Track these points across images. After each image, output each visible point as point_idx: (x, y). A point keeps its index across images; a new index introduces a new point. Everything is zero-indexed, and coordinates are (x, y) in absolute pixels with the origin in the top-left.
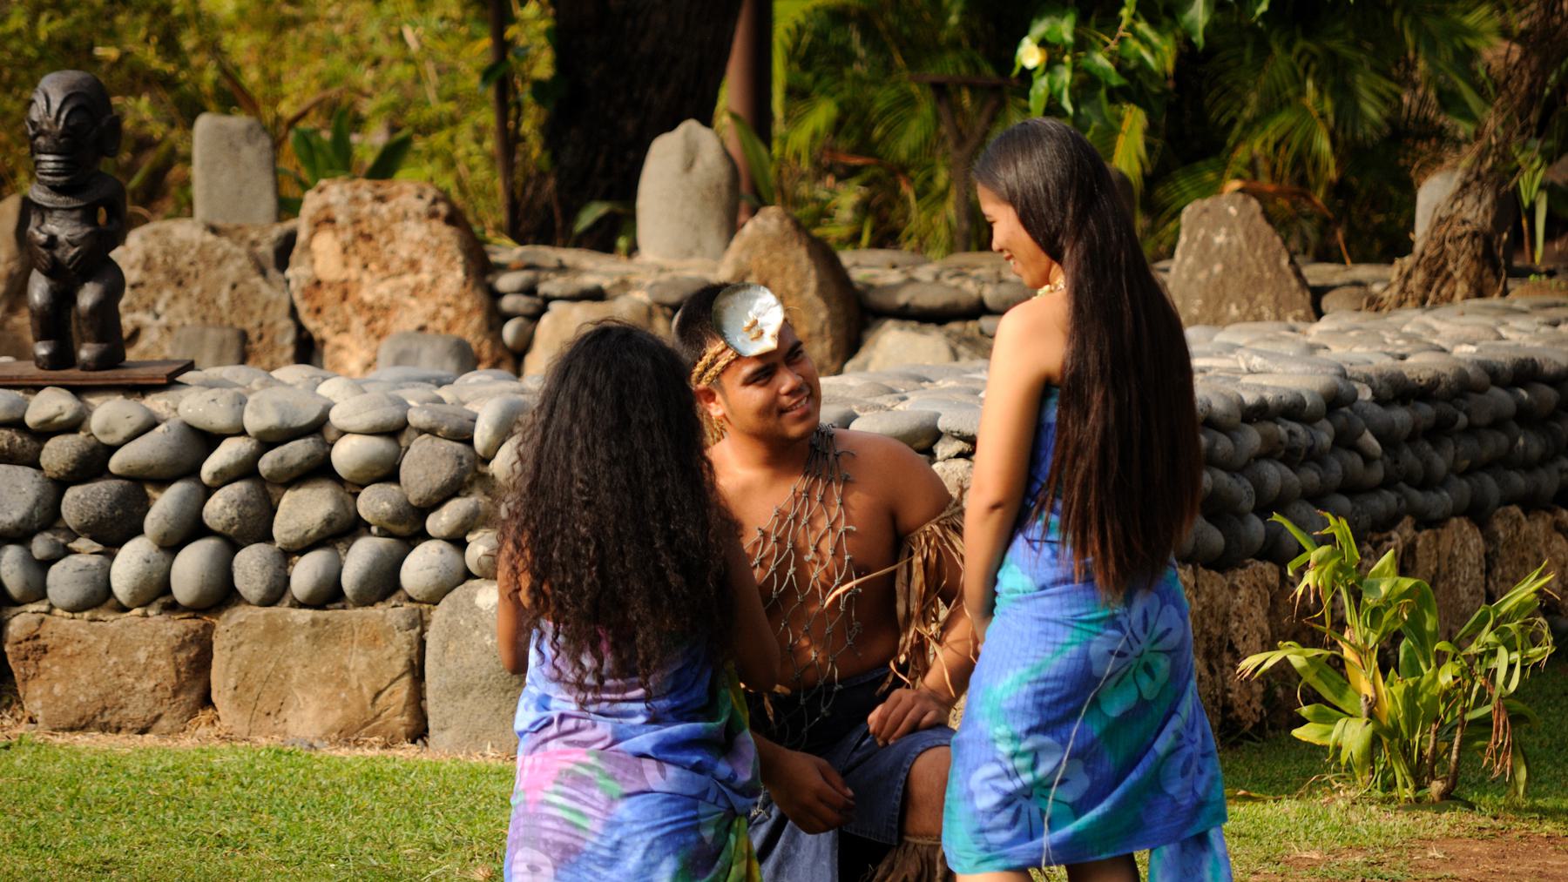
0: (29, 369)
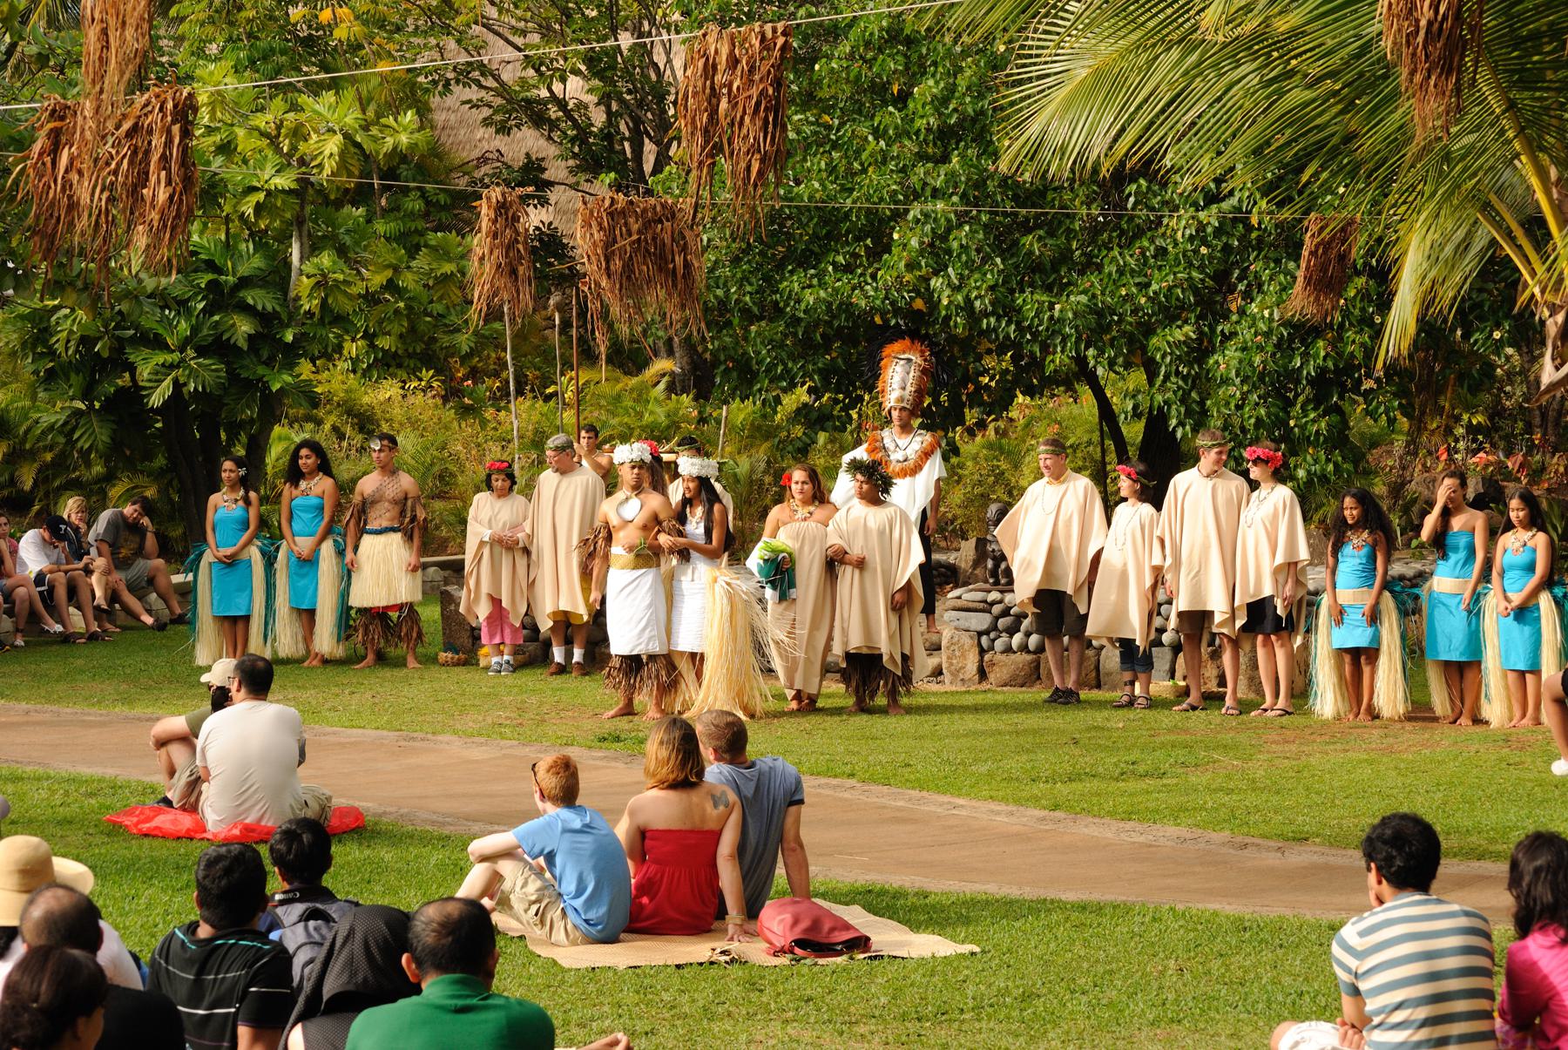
0: (987, 586)
